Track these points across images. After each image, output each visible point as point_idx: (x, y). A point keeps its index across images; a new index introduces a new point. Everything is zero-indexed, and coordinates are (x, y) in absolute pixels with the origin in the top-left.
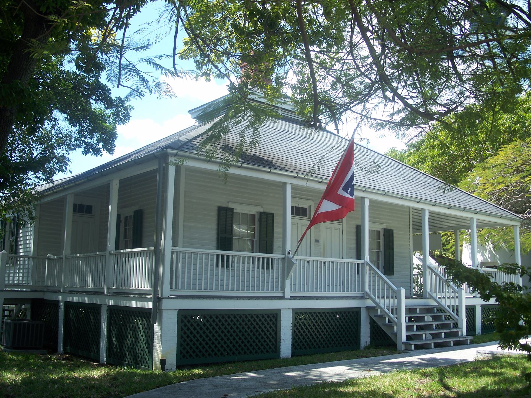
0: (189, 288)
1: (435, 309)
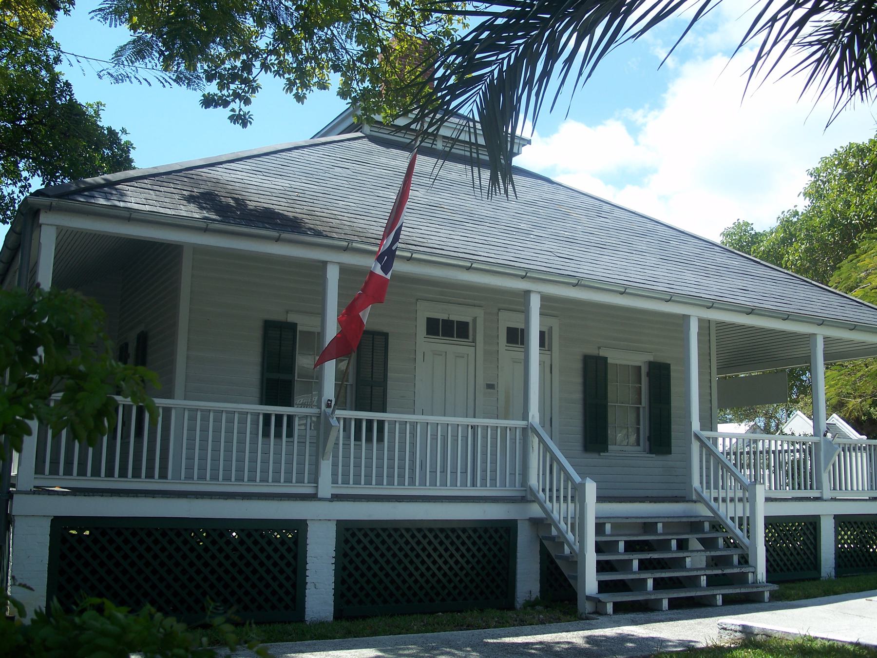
0: (189, 477)
1: (707, 525)
